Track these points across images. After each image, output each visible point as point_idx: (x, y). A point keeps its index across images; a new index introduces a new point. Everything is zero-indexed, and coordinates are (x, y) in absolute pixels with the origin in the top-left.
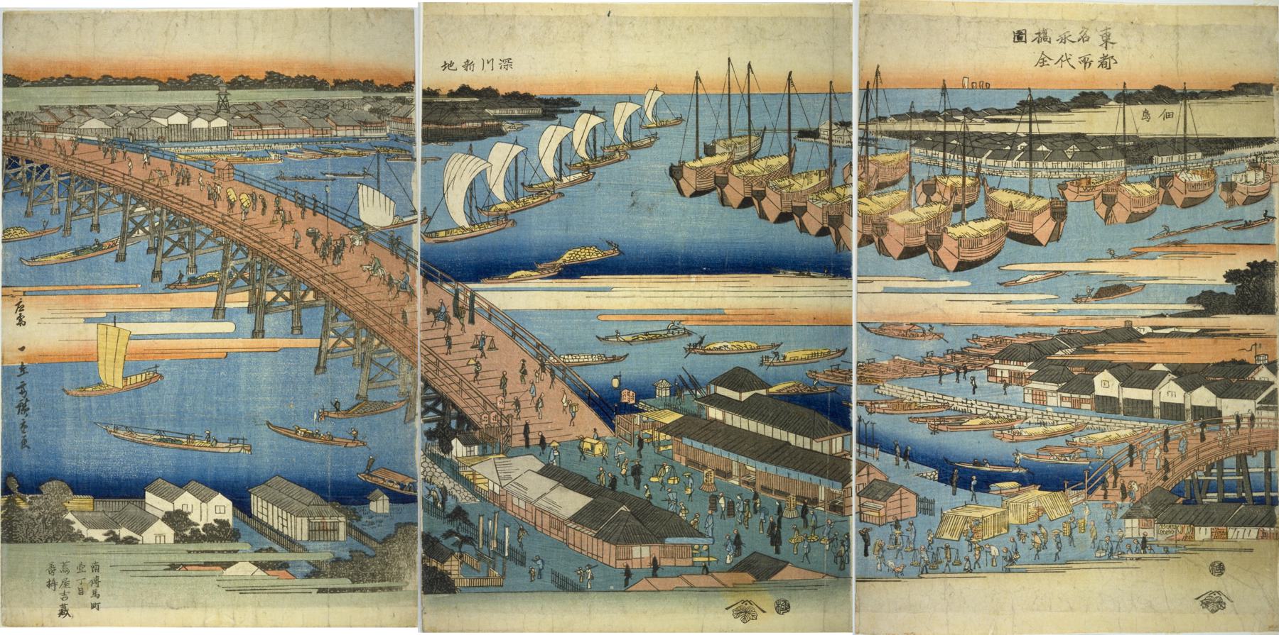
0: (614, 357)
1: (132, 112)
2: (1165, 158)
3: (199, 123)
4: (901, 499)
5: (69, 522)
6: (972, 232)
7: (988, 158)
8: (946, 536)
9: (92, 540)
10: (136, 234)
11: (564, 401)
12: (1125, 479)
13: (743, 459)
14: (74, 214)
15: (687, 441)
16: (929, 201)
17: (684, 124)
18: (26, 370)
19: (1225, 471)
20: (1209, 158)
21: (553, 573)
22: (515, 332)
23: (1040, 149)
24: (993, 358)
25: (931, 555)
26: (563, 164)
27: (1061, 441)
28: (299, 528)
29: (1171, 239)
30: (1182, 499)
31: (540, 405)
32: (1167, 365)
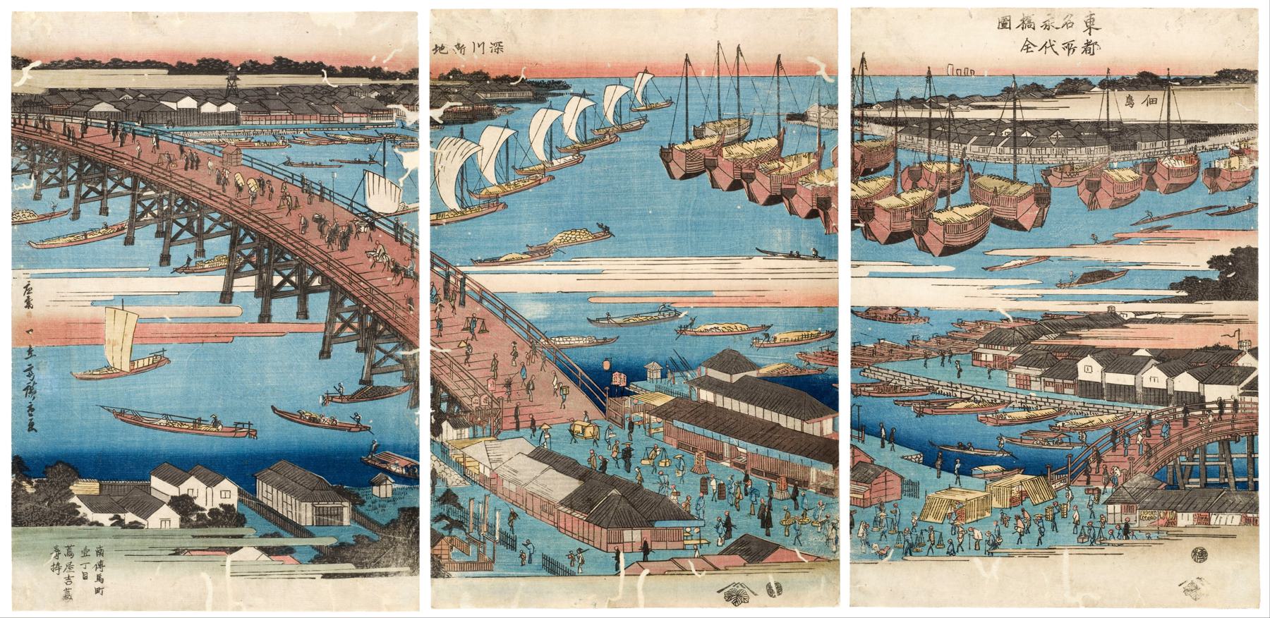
0: (605, 339)
1: (141, 96)
2: (1148, 144)
3: (209, 108)
4: (886, 481)
5: (74, 505)
6: (957, 218)
7: (972, 144)
8: (930, 519)
9: (97, 524)
10: (145, 218)
11: (555, 383)
12: (1107, 464)
13: (734, 441)
14: (84, 197)
15: (678, 423)
16: (915, 187)
17: (673, 107)
18: (33, 353)
19: (1208, 456)
20: (1193, 145)
21: (544, 557)
22: (506, 312)
23: (1024, 135)
24: (978, 342)
25: (914, 537)
26: (554, 146)
27: (1044, 426)
28: (305, 514)
29: (1155, 224)
30: (1165, 484)
31: (531, 387)
32: (1150, 350)
